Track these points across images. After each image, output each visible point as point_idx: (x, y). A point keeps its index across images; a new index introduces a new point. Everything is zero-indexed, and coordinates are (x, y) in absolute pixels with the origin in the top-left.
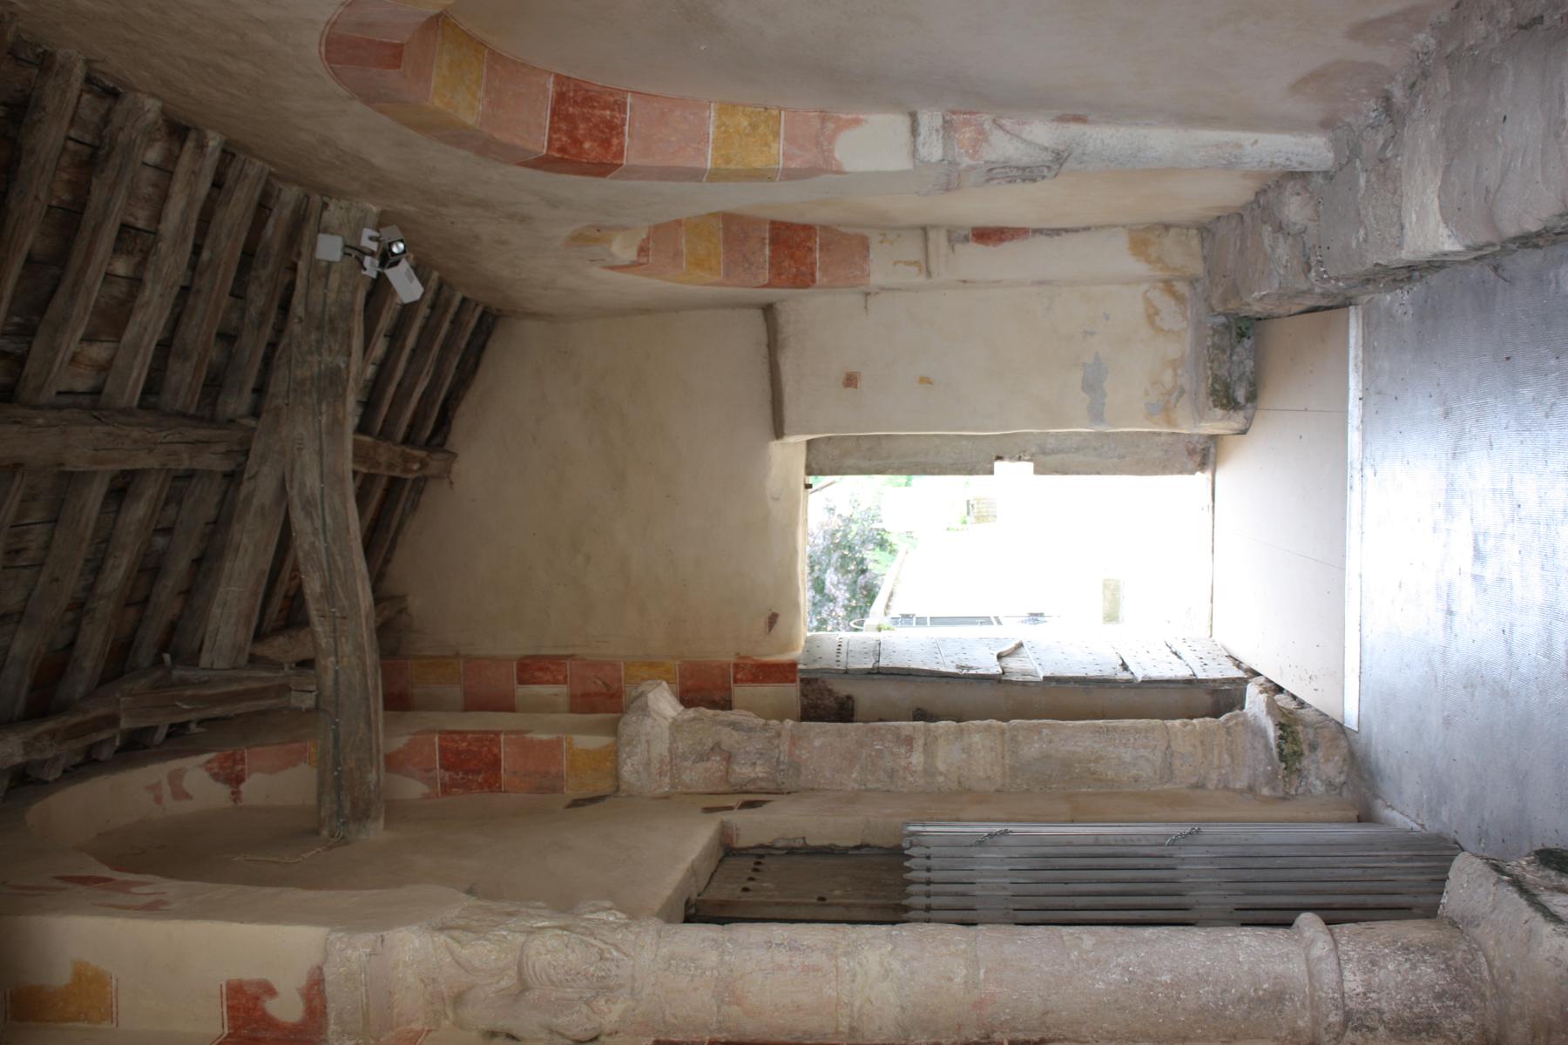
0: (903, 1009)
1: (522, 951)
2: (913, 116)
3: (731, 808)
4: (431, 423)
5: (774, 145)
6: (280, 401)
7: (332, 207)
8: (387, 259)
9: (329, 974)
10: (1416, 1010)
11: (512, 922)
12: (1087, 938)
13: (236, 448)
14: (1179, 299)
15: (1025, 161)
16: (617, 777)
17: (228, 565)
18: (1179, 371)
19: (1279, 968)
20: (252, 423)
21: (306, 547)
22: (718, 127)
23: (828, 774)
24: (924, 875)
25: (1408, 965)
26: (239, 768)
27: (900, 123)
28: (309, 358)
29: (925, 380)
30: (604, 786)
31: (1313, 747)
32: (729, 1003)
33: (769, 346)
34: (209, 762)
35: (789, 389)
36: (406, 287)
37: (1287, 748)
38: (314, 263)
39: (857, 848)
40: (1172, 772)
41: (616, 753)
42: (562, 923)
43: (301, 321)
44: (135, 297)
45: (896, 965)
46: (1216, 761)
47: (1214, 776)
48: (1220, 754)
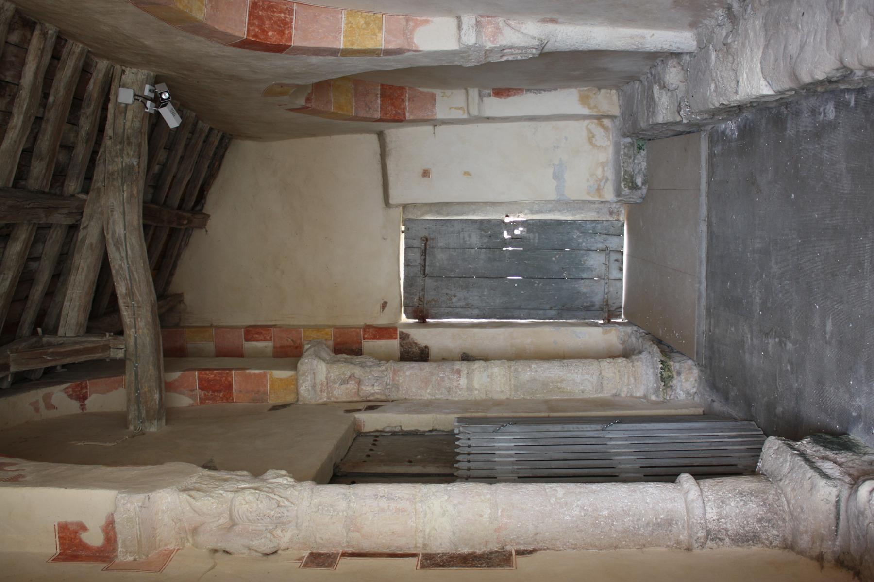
0: (454, 533)
1: (232, 502)
2: (459, 18)
3: (359, 410)
4: (194, 198)
5: (379, 35)
6: (99, 184)
7: (127, 72)
8: (158, 101)
9: (117, 519)
10: (747, 529)
11: (226, 485)
12: (559, 491)
13: (75, 211)
14: (605, 128)
15: (523, 44)
16: (297, 393)
17: (72, 278)
18: (606, 169)
19: (670, 506)
20: (83, 196)
21: (117, 267)
22: (347, 24)
23: (414, 390)
24: (467, 450)
25: (742, 503)
26: (84, 391)
27: (452, 22)
28: (116, 159)
29: (466, 173)
30: (290, 399)
31: (679, 374)
32: (353, 531)
33: (381, 155)
34: (66, 388)
35: (392, 179)
36: (171, 119)
37: (665, 374)
38: (117, 105)
39: (430, 431)
40: (602, 387)
41: (297, 380)
42: (255, 485)
43: (111, 138)
44: (7, 123)
45: (450, 508)
46: (626, 381)
47: (625, 389)
48: (629, 378)
